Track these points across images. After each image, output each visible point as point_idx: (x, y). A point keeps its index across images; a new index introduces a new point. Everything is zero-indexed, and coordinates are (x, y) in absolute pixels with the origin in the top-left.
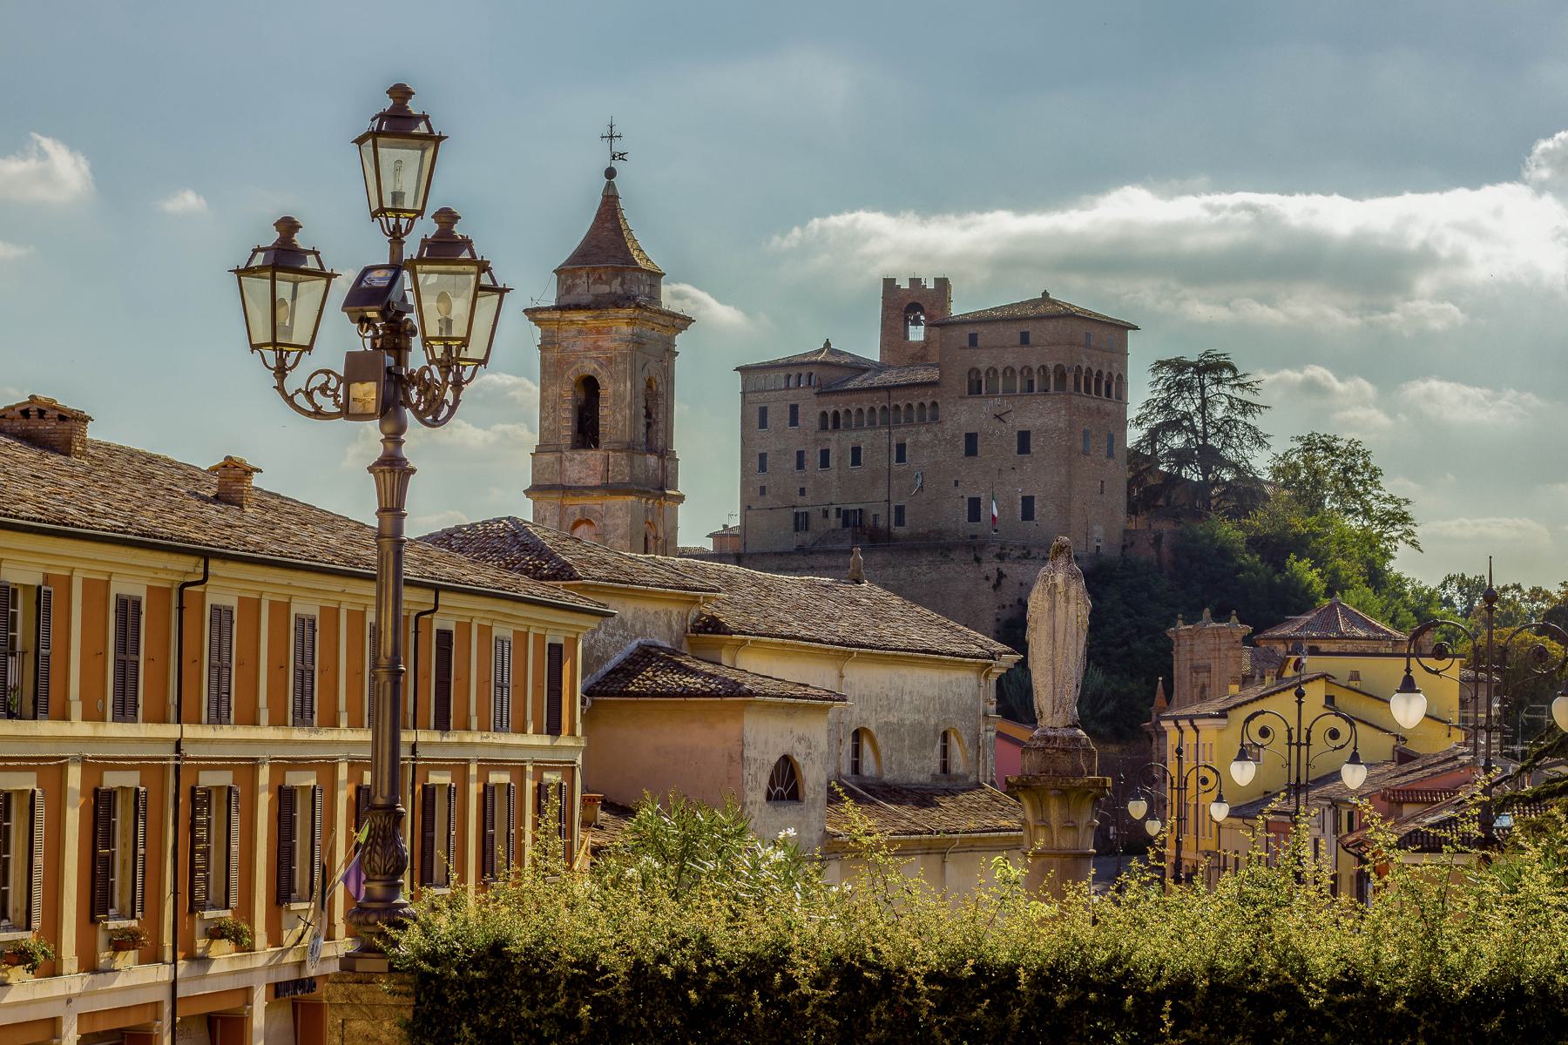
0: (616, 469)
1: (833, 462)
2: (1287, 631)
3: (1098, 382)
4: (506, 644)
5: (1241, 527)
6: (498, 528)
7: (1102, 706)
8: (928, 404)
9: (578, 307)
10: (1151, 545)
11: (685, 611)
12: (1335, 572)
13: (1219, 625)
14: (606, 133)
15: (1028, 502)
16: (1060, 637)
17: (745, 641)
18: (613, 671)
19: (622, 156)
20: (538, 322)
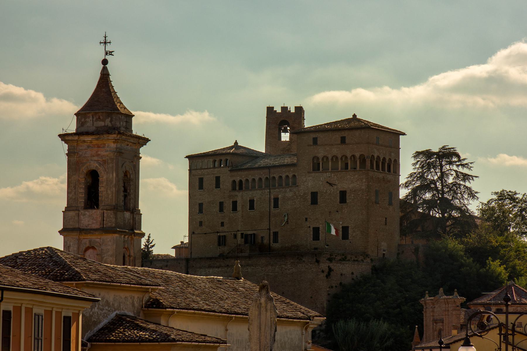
0: (108, 220)
1: (239, 208)
2: (484, 300)
3: (383, 164)
4: (40, 317)
5: (462, 243)
6: (42, 253)
7: (386, 341)
8: (290, 176)
9: (87, 134)
10: (413, 253)
11: (142, 296)
12: (514, 267)
13: (448, 297)
14: (103, 40)
16: (263, 327)
17: (173, 312)
18: (103, 329)
19: (111, 53)
20: (66, 142)
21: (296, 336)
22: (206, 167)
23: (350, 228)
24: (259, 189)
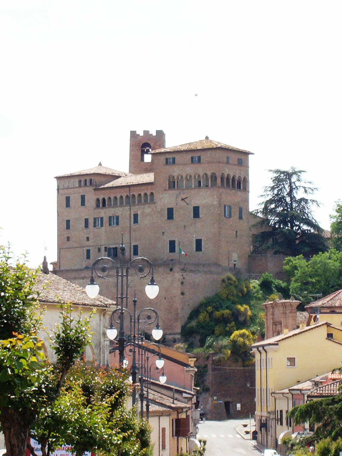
8: (149, 194)
15: (199, 242)
22: (73, 187)
24: (120, 207)
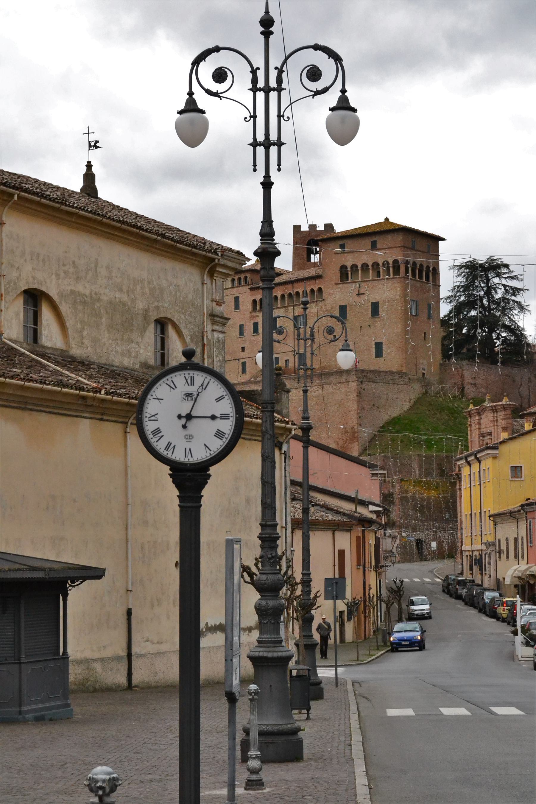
1: (260, 330)
15: (379, 346)
21: (187, 283)
23: (383, 343)
